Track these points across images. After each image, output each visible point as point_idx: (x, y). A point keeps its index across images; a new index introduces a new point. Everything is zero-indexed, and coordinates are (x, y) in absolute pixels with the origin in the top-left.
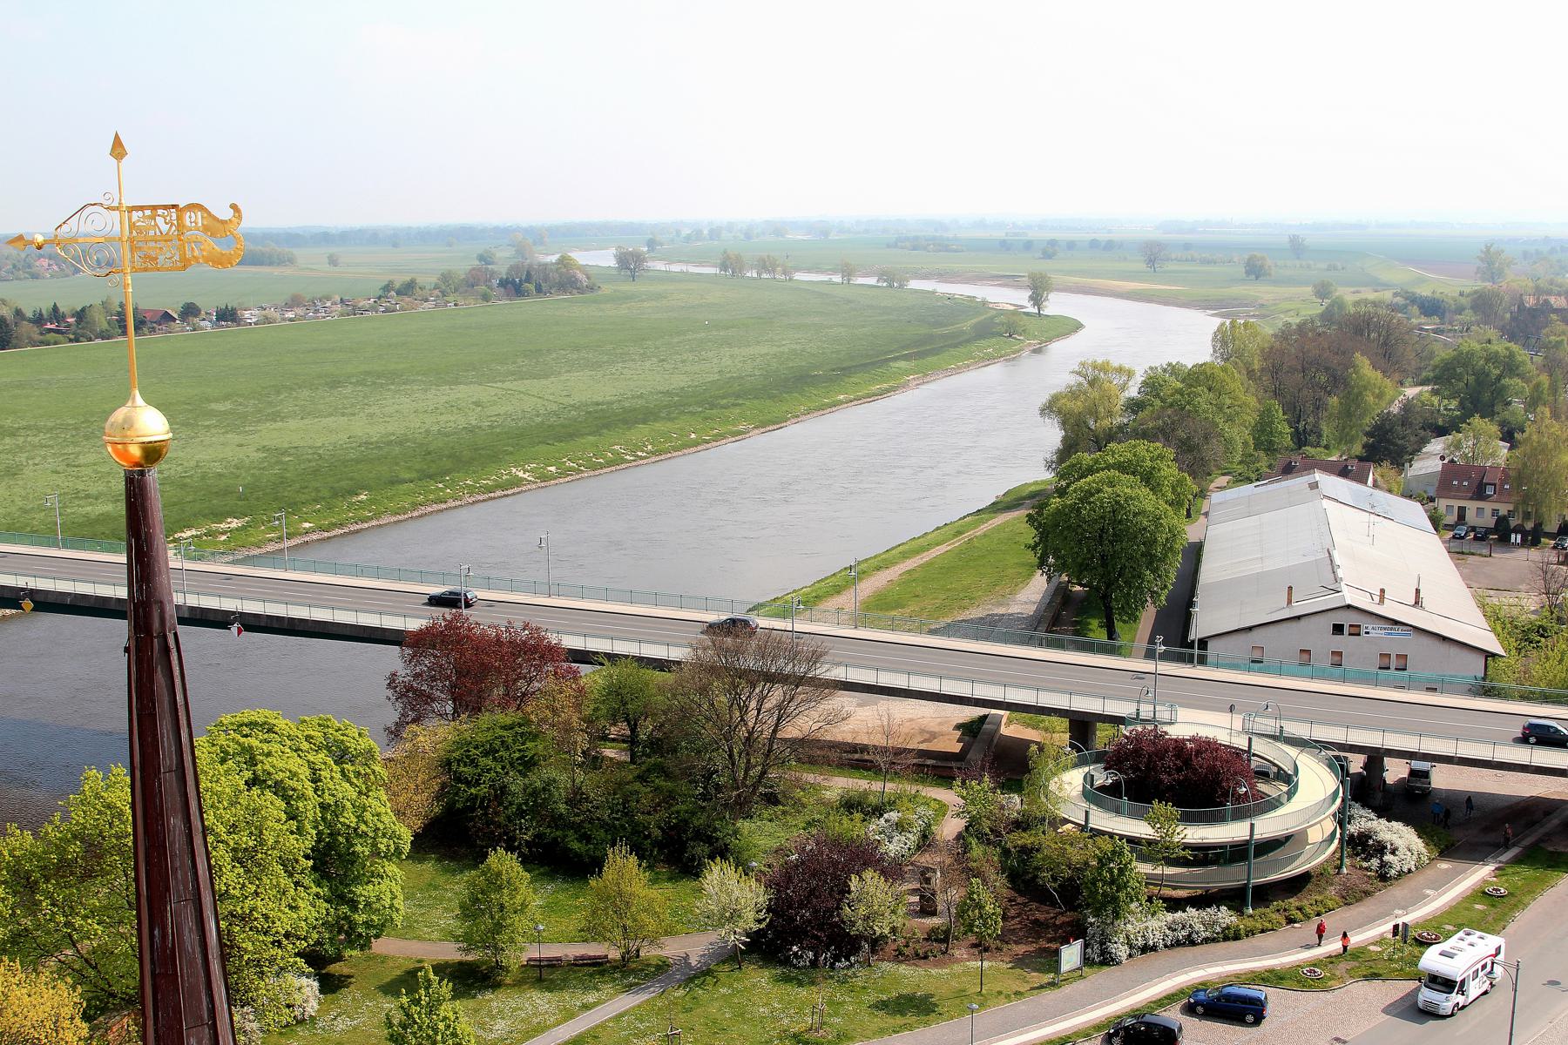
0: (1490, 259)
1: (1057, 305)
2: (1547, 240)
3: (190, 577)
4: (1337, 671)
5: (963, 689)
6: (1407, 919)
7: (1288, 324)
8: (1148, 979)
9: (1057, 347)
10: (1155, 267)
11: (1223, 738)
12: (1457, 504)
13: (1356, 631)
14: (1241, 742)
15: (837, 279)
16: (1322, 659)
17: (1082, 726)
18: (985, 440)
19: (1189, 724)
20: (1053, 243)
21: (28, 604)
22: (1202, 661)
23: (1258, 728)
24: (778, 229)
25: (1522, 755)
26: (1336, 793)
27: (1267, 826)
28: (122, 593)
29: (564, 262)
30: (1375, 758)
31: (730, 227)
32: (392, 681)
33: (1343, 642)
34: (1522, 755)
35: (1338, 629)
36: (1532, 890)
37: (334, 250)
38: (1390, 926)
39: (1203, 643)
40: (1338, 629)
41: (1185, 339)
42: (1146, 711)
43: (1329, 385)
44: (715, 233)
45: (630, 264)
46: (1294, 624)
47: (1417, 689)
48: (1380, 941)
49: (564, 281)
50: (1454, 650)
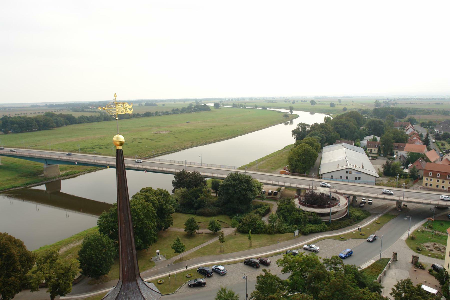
0: (377, 103)
1: (295, 112)
2: (388, 99)
3: (128, 162)
4: (347, 180)
5: (277, 183)
6: (360, 227)
7: (338, 116)
8: (311, 238)
9: (294, 120)
10: (312, 106)
11: (325, 192)
12: (370, 149)
13: (351, 173)
14: (329, 194)
15: (288, 111)
16: (344, 178)
17: (299, 190)
18: (280, 138)
19: (320, 190)
20: (294, 101)
21: (108, 167)
22: (321, 178)
23: (332, 191)
24: (243, 99)
25: (383, 196)
26: (347, 203)
27: (334, 209)
28: (115, 163)
29: (205, 105)
30: (355, 197)
31: (235, 99)
32: (173, 181)
33: (348, 175)
34: (383, 196)
35: (347, 172)
36: (384, 223)
37: (163, 103)
38: (357, 228)
39: (322, 175)
40: (347, 172)
41: (319, 119)
42: (311, 187)
43: (346, 127)
44: (232, 100)
45: (217, 106)
46: (339, 172)
47: (363, 184)
48: (355, 231)
49: (205, 108)
50: (370, 176)
